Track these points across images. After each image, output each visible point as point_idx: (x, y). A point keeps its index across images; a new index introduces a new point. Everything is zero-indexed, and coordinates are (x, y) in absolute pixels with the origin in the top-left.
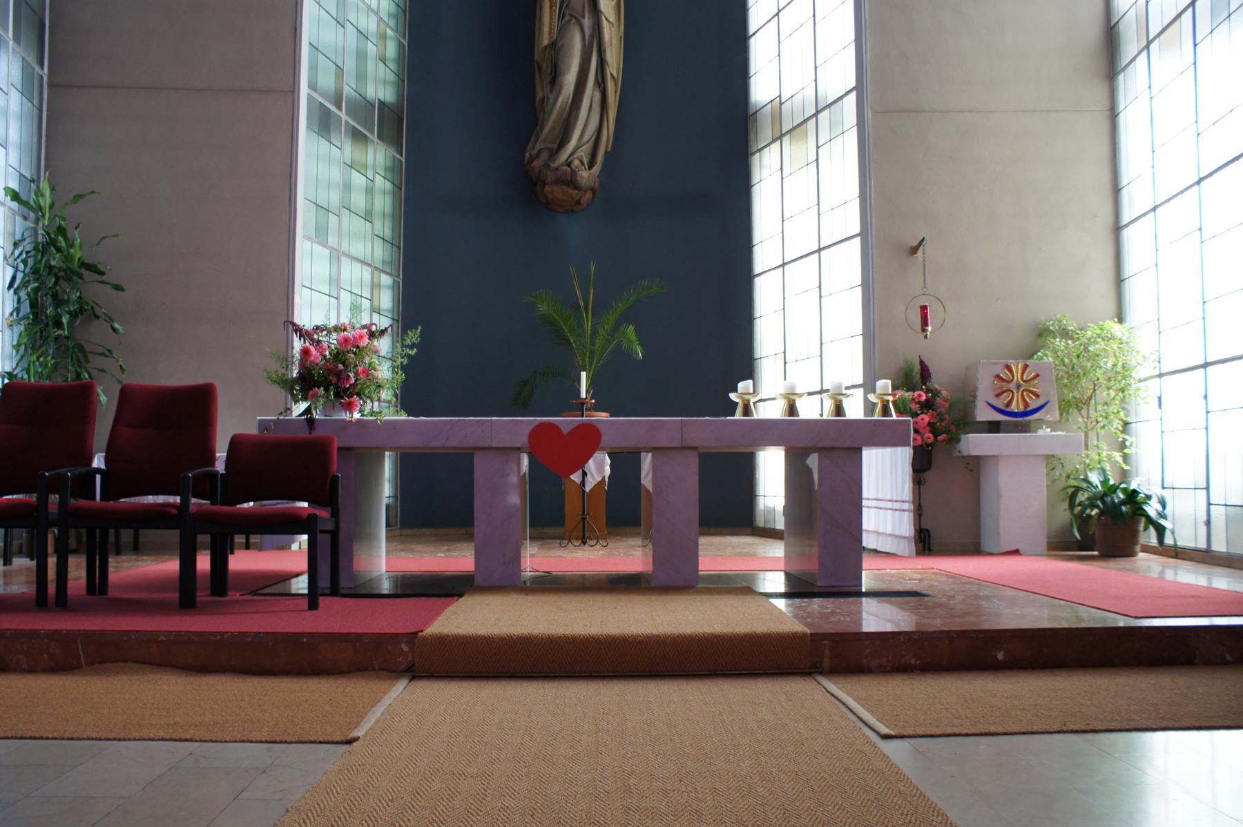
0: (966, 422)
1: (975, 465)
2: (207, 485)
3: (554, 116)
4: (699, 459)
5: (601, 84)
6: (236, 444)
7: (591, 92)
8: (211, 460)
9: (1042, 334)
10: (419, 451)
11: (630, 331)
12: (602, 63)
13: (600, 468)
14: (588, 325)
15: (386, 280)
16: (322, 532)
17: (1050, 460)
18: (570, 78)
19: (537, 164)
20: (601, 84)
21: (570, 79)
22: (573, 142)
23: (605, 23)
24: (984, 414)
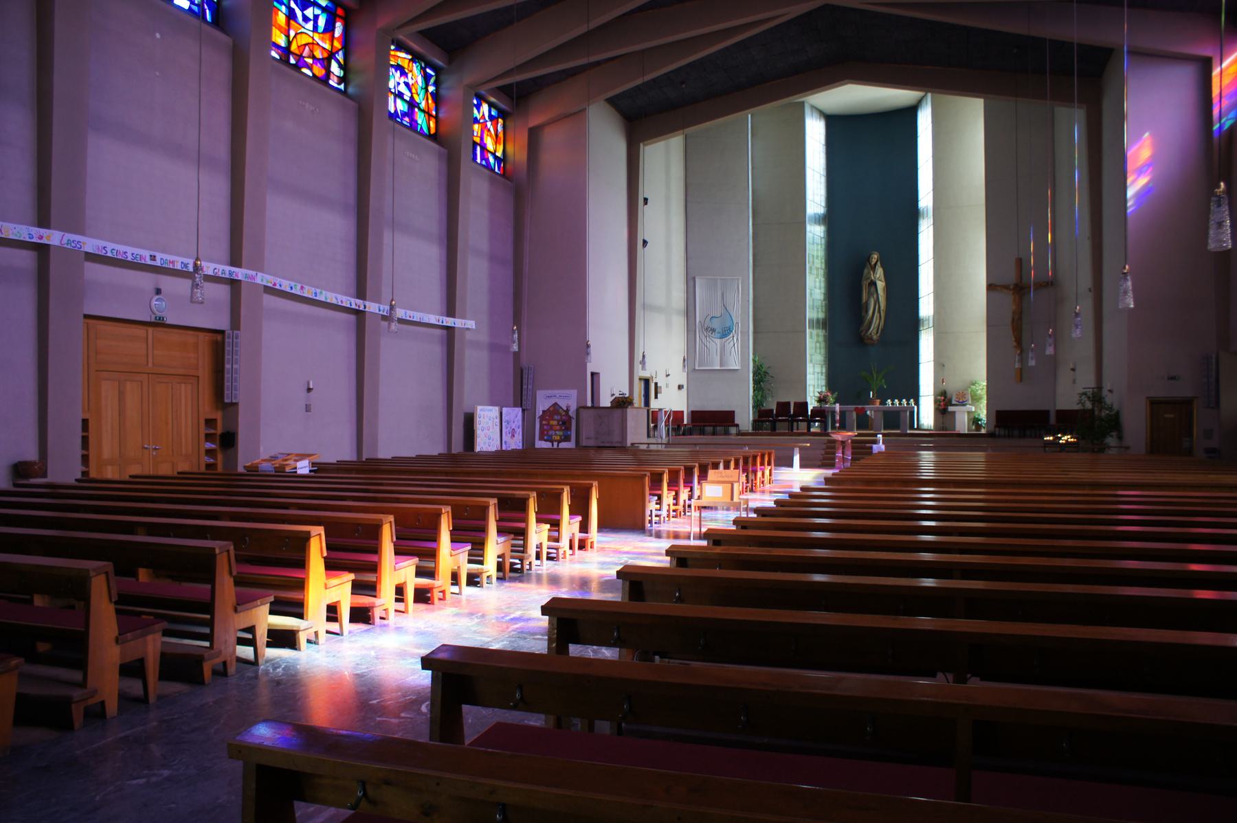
1: (954, 413)
2: (790, 416)
4: (509, 651)
5: (879, 312)
6: (812, 411)
8: (790, 412)
11: (883, 381)
16: (553, 445)
17: (969, 413)
19: (862, 334)
20: (879, 312)
21: (871, 312)
22: (871, 329)
23: (880, 296)
24: (954, 402)
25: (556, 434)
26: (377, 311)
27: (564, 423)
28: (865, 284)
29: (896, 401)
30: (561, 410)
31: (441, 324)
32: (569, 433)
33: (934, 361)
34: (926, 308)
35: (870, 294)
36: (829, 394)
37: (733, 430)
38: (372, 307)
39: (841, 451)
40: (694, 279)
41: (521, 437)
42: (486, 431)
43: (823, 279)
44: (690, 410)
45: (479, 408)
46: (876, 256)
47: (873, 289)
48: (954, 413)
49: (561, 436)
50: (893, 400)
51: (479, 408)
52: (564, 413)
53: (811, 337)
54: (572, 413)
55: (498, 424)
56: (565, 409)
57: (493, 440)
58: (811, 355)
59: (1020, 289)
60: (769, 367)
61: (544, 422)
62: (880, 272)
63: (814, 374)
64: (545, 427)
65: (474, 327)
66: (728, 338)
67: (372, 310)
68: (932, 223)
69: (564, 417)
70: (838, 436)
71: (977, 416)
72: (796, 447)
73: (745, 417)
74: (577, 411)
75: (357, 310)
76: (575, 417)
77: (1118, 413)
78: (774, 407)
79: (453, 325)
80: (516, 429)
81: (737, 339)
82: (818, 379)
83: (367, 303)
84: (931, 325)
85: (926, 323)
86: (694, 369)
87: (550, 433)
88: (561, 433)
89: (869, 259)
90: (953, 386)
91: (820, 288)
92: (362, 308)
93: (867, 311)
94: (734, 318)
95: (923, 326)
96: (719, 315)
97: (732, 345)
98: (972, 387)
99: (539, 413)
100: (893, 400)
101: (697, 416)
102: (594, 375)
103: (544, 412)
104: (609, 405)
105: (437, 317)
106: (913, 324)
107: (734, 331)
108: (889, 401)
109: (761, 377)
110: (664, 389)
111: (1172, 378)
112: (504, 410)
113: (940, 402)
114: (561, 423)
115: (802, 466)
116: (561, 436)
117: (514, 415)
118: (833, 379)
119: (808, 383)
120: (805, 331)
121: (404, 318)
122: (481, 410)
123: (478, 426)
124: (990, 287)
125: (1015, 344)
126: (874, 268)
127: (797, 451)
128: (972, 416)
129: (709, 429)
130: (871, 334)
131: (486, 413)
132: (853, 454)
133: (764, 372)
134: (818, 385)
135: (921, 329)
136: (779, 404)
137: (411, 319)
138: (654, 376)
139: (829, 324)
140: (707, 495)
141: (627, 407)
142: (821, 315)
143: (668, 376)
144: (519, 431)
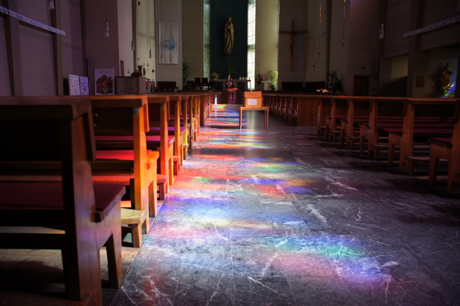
1: (264, 83)
5: (231, 42)
7: (230, 43)
10: (420, 143)
11: (234, 71)
12: (232, 40)
14: (230, 69)
20: (231, 42)
24: (263, 79)
25: (105, 90)
26: (16, 17)
27: (109, 84)
28: (226, 30)
29: (243, 78)
30: (107, 78)
31: (50, 30)
32: (111, 89)
34: (251, 40)
35: (228, 35)
36: (216, 74)
37: (175, 90)
38: (13, 14)
40: (158, 23)
41: (88, 91)
42: (74, 87)
43: (209, 27)
44: (157, 81)
45: (71, 75)
46: (231, 19)
47: (229, 32)
48: (264, 83)
49: (107, 91)
50: (242, 78)
51: (71, 75)
52: (108, 80)
53: (205, 52)
54: (113, 79)
55: (79, 84)
56: (109, 78)
57: (77, 92)
59: (293, 33)
61: (99, 84)
62: (232, 25)
64: (100, 86)
65: (65, 35)
67: (13, 15)
68: (255, 5)
69: (108, 82)
70: (231, 90)
72: (215, 94)
73: (180, 85)
74: (116, 78)
75: (3, 13)
76: (114, 82)
77: (340, 81)
79: (55, 32)
80: (86, 87)
81: (177, 51)
83: (10, 11)
84: (254, 47)
86: (159, 63)
87: (102, 89)
88: (108, 89)
89: (228, 20)
90: (263, 72)
91: (208, 31)
92: (7, 13)
93: (227, 42)
95: (249, 48)
99: (96, 80)
100: (242, 78)
101: (159, 83)
102: (122, 62)
103: (98, 79)
104: (130, 76)
105: (48, 26)
106: (245, 48)
109: (185, 68)
110: (147, 72)
111: (363, 68)
112: (81, 78)
114: (107, 84)
116: (107, 91)
117: (85, 80)
118: (212, 70)
120: (203, 49)
121: (31, 23)
122: (71, 77)
123: (70, 84)
124: (281, 32)
125: (291, 55)
126: (230, 24)
127: (216, 95)
128: (270, 85)
129: (165, 89)
131: (74, 78)
135: (249, 50)
136: (195, 78)
137: (35, 25)
138: (143, 65)
139: (211, 47)
141: (139, 77)
142: (208, 43)
143: (148, 66)
144: (87, 88)
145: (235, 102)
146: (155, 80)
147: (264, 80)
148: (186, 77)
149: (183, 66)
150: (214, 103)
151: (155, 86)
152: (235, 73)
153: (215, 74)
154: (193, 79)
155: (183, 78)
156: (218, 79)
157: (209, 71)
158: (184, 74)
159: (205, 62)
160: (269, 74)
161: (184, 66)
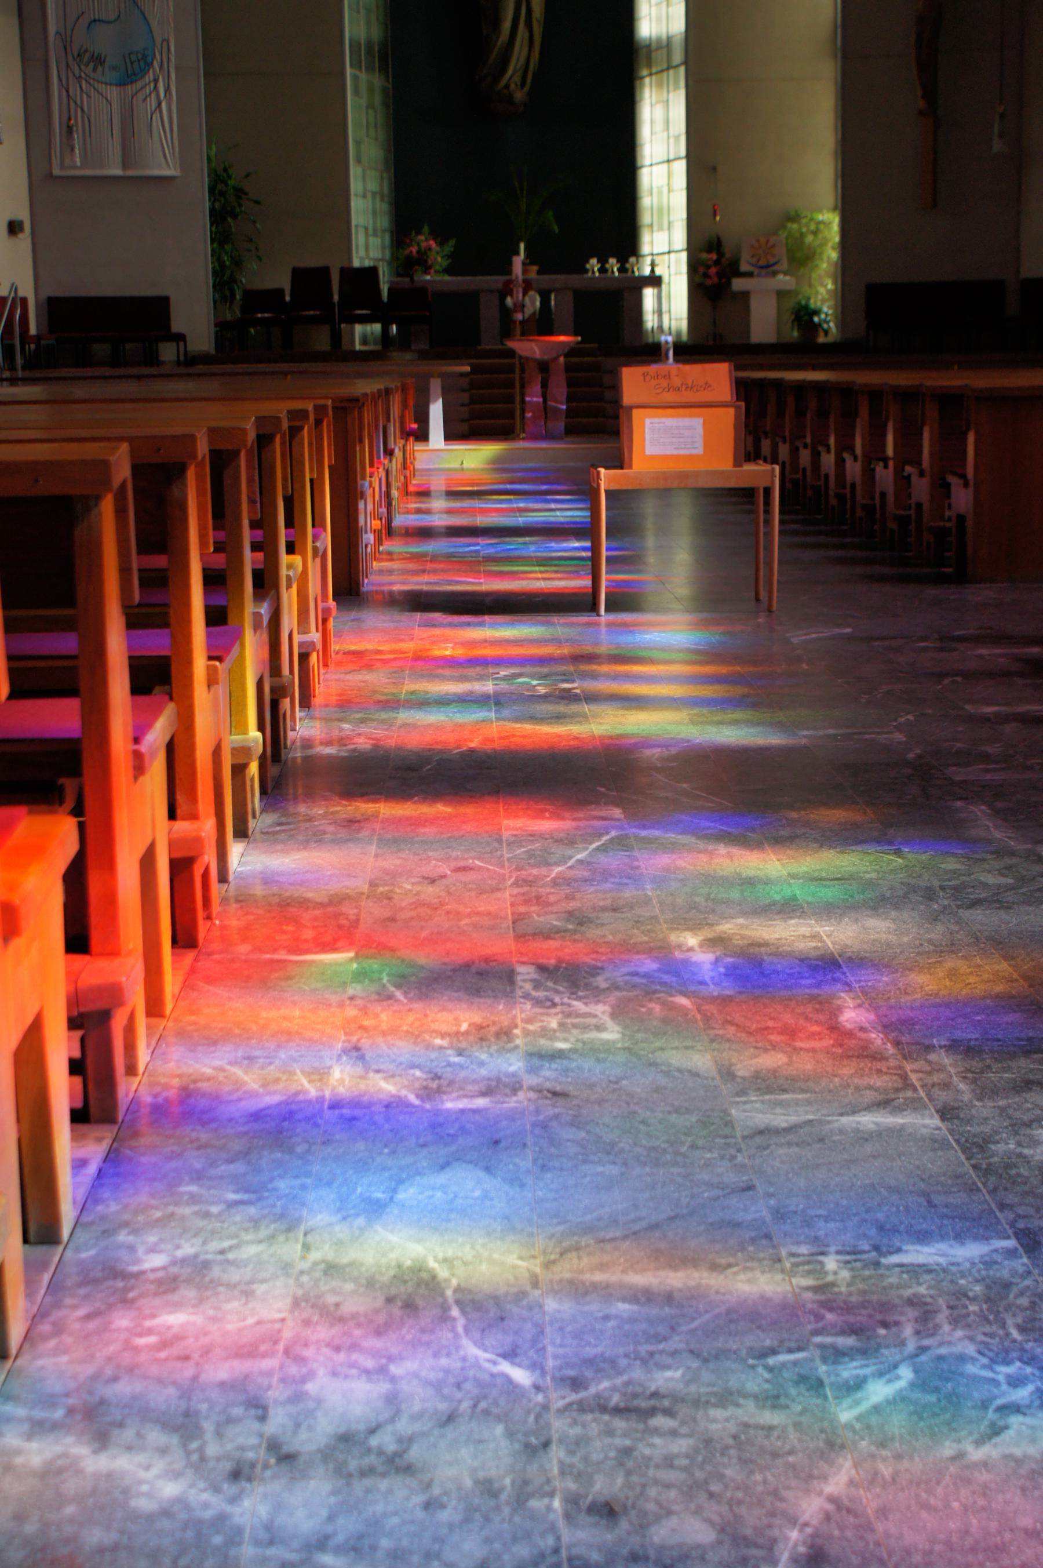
0: (732, 269)
1: (745, 295)
3: (496, 50)
6: (390, 290)
9: (795, 218)
13: (533, 302)
14: (523, 207)
15: (385, 175)
18: (507, 25)
21: (507, 25)
24: (744, 267)
29: (612, 261)
33: (689, 157)
36: (432, 243)
37: (168, 352)
39: (537, 388)
48: (745, 295)
50: (603, 261)
53: (356, 92)
58: (358, 143)
60: (248, 175)
63: (364, 196)
66: (139, 84)
70: (531, 348)
71: (803, 302)
78: (282, 281)
81: (167, 89)
82: (374, 213)
84: (678, 57)
85: (659, 56)
86: (50, 175)
93: (496, 23)
94: (154, 25)
95: (649, 65)
96: (112, 18)
97: (154, 105)
98: (789, 225)
100: (603, 261)
107: (156, 65)
108: (594, 261)
113: (708, 267)
115: (450, 436)
119: (354, 223)
125: (921, 104)
127: (436, 385)
128: (790, 304)
129: (101, 349)
130: (507, 86)
132: (570, 399)
133: (234, 188)
134: (375, 230)
135: (644, 72)
136: (298, 274)
140: (650, 450)
142: (376, 33)
145: (561, 425)
146: (27, 290)
147: (749, 275)
148: (238, 263)
149: (212, 191)
150: (422, 436)
151: (33, 331)
152: (556, 229)
153: (423, 241)
154: (282, 281)
155: (215, 273)
156: (448, 271)
157: (384, 222)
158: (221, 245)
159: (358, 160)
160: (783, 234)
161: (222, 194)
